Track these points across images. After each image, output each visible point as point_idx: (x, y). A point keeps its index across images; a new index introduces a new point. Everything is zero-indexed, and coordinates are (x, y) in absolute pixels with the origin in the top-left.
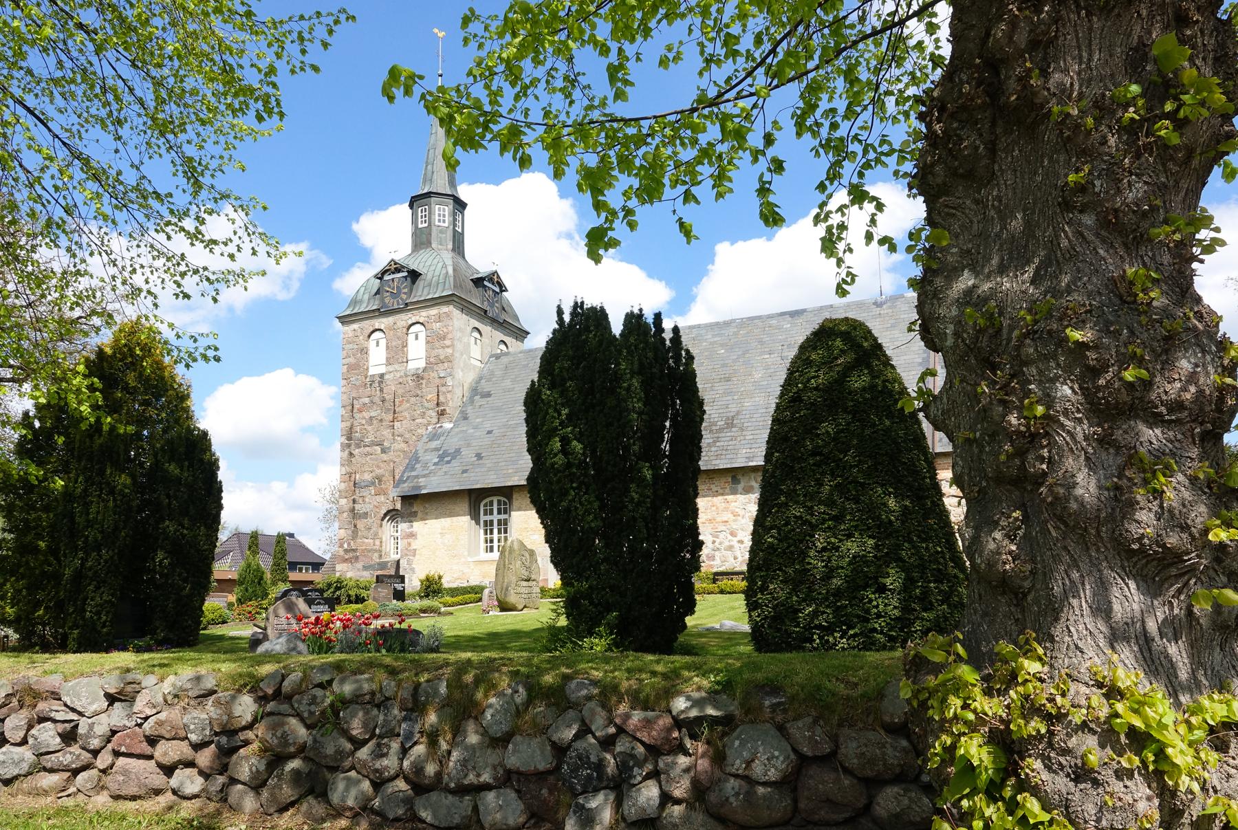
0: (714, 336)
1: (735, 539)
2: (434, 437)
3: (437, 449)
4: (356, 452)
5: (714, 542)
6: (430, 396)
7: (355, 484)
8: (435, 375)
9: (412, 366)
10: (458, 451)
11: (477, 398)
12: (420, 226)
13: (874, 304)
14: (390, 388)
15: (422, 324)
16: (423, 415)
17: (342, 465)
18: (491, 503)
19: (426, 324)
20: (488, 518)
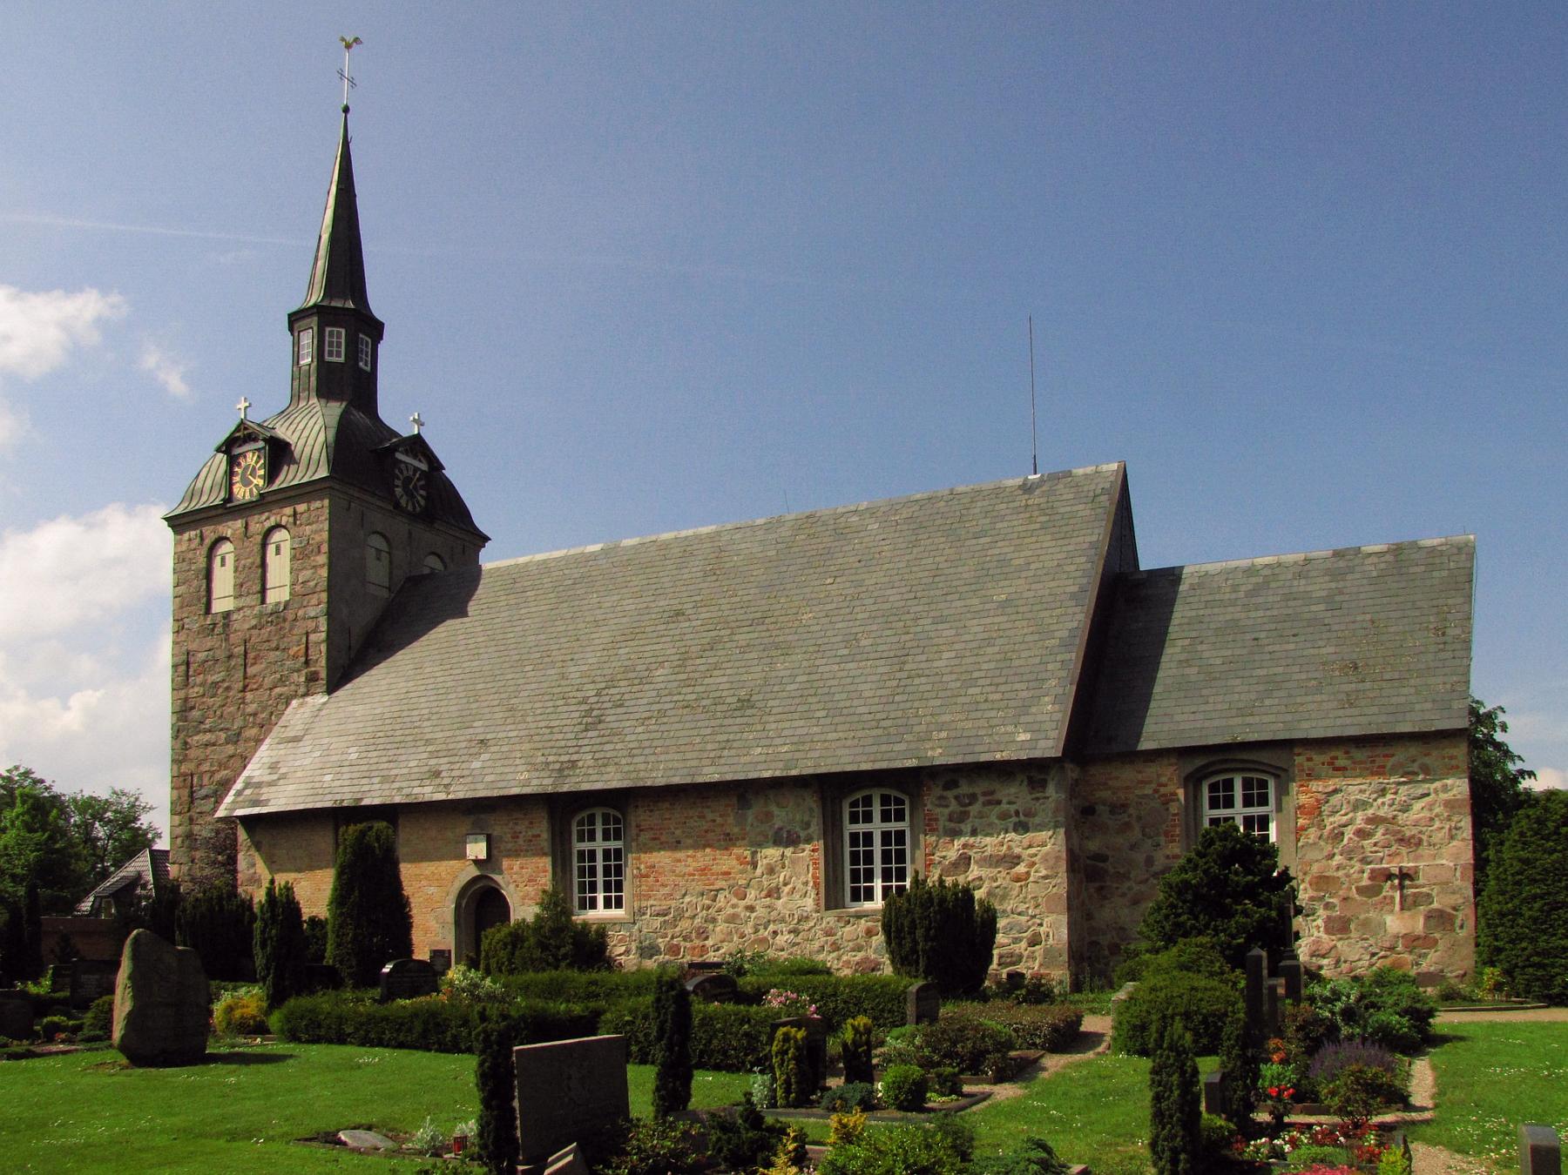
6: (296, 649)
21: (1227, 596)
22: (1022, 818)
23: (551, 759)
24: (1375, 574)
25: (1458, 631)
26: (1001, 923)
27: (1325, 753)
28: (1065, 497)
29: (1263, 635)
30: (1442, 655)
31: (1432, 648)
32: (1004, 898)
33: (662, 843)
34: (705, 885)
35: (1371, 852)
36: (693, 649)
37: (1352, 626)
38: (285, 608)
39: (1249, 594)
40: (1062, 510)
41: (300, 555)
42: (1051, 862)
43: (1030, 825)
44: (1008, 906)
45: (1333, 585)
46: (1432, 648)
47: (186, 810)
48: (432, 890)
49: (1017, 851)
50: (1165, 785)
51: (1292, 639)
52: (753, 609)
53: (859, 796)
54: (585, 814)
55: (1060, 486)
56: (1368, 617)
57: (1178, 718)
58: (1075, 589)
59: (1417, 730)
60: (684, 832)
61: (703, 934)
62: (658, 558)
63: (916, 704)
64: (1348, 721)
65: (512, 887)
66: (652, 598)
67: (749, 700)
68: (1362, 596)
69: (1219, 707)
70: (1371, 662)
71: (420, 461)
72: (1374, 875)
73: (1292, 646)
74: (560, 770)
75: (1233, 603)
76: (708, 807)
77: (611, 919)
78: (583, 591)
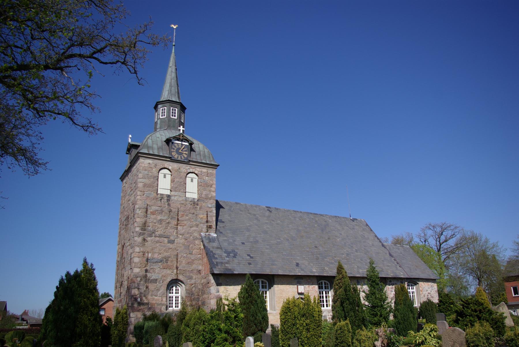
15: (196, 174)
18: (258, 282)
19: (200, 176)
20: (177, 295)
38: (198, 201)
47: (144, 266)
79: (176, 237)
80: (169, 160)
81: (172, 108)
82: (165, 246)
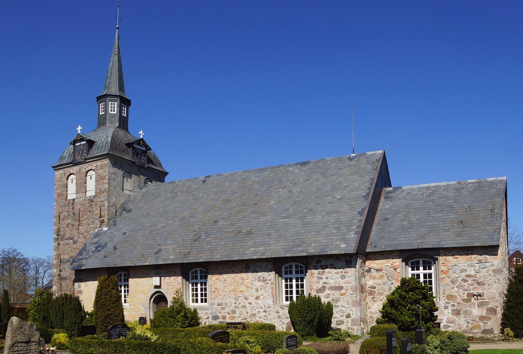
0: (256, 177)
1: (247, 302)
2: (97, 235)
3: (96, 243)
4: (61, 243)
5: (235, 303)
6: (97, 212)
7: (61, 261)
8: (98, 199)
9: (89, 194)
10: (106, 244)
11: (124, 212)
12: (101, 114)
13: (348, 158)
14: (77, 207)
16: (93, 223)
17: (55, 250)
18: (196, 272)
21: (419, 197)
22: (343, 273)
23: (182, 251)
24: (471, 190)
25: (498, 211)
26: (334, 311)
27: (450, 252)
28: (363, 162)
29: (431, 211)
30: (492, 219)
31: (489, 216)
32: (337, 301)
33: (220, 281)
34: (235, 295)
35: (467, 287)
36: (233, 213)
37: (462, 208)
38: (93, 198)
39: (427, 196)
40: (362, 167)
41: (99, 179)
42: (354, 289)
43: (346, 276)
44: (339, 304)
45: (456, 194)
46: (489, 216)
47: (59, 267)
48: (141, 296)
49: (342, 285)
50: (395, 263)
51: (441, 212)
52: (254, 200)
53: (288, 265)
54: (194, 270)
55: (362, 158)
56: (468, 205)
57: (399, 239)
58: (365, 194)
59: (482, 245)
60: (227, 277)
61: (234, 312)
62: (223, 181)
63: (307, 234)
64: (458, 242)
65: (169, 294)
66: (220, 195)
67: (250, 232)
68: (466, 198)
69: (414, 235)
70: (468, 221)
71: (143, 147)
72: (469, 295)
73: (441, 215)
74: (185, 255)
75: (421, 199)
76: (236, 268)
77: (202, 306)
78: (197, 192)
79: (78, 237)
80: (72, 165)
81: (110, 102)
82: (71, 247)
